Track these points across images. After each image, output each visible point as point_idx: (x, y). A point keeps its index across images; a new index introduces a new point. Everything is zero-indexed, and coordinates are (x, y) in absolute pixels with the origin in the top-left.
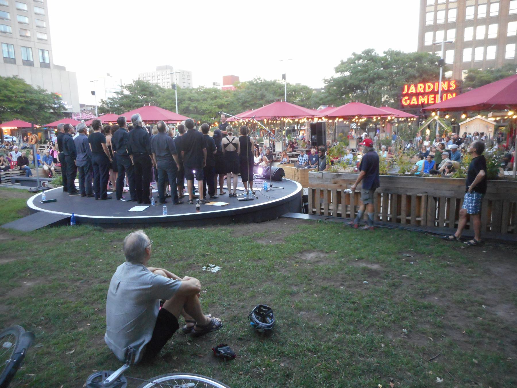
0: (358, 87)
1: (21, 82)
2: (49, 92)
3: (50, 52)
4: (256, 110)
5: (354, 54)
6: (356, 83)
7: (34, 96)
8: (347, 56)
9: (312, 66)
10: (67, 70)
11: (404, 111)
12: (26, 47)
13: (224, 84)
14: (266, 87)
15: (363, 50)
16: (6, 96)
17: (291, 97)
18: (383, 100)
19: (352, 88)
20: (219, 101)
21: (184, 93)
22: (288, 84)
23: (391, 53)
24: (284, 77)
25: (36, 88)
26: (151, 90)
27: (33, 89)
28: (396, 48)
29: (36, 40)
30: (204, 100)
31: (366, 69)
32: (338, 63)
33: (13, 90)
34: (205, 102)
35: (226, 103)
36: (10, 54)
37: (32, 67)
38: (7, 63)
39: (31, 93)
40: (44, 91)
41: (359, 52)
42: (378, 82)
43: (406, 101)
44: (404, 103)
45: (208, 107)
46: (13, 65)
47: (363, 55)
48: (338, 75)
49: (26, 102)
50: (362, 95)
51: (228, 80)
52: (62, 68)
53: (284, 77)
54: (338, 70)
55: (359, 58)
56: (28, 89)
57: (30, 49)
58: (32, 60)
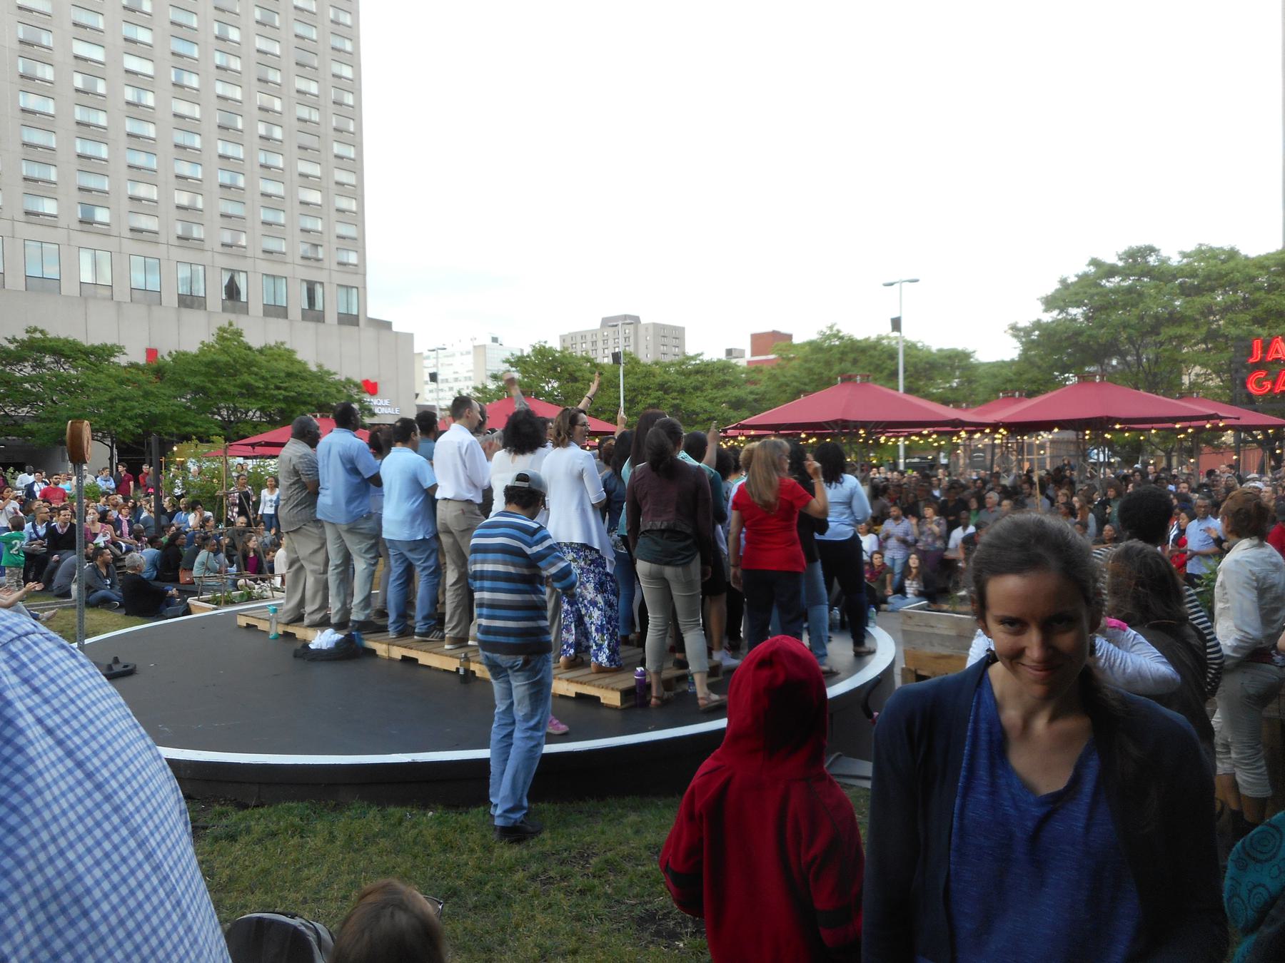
0: (1111, 348)
1: (289, 355)
2: (341, 377)
3: (361, 290)
4: (1054, 393)
5: (1095, 262)
6: (1103, 335)
7: (304, 387)
8: (1075, 268)
9: (982, 314)
10: (395, 328)
11: (1256, 410)
12: (274, 277)
13: (753, 354)
14: (852, 356)
15: (1123, 248)
16: (248, 386)
17: (918, 379)
18: (1186, 380)
19: (1099, 353)
20: (734, 392)
21: (649, 374)
22: (910, 347)
23: (1204, 254)
24: (896, 324)
25: (314, 368)
26: (571, 368)
27: (306, 370)
28: (1220, 240)
29: (335, 267)
30: (696, 389)
31: (1132, 297)
32: (1052, 287)
33: (264, 372)
34: (699, 393)
35: (752, 397)
36: (278, 298)
37: (321, 326)
38: (271, 316)
39: (304, 379)
40: (329, 373)
41: (1111, 258)
42: (1167, 332)
43: (1260, 384)
44: (1252, 388)
45: (706, 404)
46: (281, 321)
47: (1121, 264)
48: (1048, 317)
49: (286, 399)
50: (1122, 371)
51: (761, 342)
52: (387, 325)
53: (896, 324)
54: (1050, 303)
55: (1111, 271)
56: (295, 369)
57: (355, 291)
58: (355, 312)
